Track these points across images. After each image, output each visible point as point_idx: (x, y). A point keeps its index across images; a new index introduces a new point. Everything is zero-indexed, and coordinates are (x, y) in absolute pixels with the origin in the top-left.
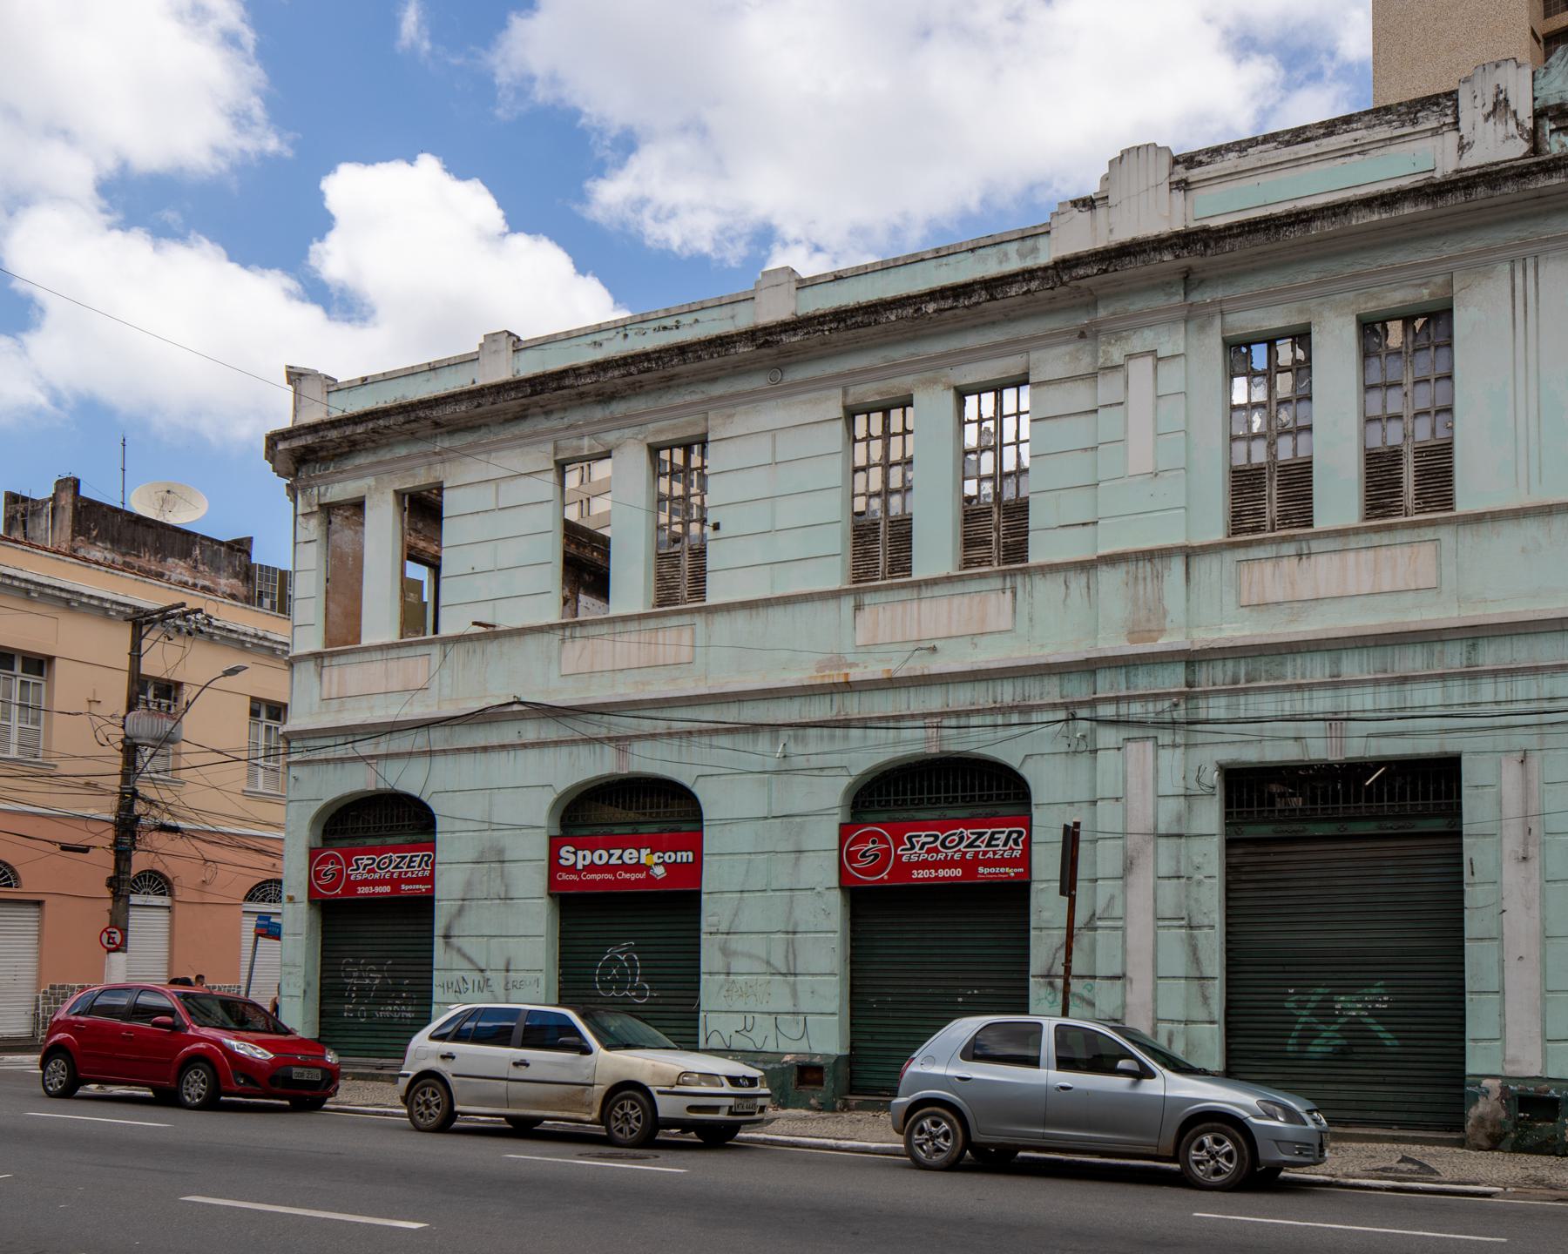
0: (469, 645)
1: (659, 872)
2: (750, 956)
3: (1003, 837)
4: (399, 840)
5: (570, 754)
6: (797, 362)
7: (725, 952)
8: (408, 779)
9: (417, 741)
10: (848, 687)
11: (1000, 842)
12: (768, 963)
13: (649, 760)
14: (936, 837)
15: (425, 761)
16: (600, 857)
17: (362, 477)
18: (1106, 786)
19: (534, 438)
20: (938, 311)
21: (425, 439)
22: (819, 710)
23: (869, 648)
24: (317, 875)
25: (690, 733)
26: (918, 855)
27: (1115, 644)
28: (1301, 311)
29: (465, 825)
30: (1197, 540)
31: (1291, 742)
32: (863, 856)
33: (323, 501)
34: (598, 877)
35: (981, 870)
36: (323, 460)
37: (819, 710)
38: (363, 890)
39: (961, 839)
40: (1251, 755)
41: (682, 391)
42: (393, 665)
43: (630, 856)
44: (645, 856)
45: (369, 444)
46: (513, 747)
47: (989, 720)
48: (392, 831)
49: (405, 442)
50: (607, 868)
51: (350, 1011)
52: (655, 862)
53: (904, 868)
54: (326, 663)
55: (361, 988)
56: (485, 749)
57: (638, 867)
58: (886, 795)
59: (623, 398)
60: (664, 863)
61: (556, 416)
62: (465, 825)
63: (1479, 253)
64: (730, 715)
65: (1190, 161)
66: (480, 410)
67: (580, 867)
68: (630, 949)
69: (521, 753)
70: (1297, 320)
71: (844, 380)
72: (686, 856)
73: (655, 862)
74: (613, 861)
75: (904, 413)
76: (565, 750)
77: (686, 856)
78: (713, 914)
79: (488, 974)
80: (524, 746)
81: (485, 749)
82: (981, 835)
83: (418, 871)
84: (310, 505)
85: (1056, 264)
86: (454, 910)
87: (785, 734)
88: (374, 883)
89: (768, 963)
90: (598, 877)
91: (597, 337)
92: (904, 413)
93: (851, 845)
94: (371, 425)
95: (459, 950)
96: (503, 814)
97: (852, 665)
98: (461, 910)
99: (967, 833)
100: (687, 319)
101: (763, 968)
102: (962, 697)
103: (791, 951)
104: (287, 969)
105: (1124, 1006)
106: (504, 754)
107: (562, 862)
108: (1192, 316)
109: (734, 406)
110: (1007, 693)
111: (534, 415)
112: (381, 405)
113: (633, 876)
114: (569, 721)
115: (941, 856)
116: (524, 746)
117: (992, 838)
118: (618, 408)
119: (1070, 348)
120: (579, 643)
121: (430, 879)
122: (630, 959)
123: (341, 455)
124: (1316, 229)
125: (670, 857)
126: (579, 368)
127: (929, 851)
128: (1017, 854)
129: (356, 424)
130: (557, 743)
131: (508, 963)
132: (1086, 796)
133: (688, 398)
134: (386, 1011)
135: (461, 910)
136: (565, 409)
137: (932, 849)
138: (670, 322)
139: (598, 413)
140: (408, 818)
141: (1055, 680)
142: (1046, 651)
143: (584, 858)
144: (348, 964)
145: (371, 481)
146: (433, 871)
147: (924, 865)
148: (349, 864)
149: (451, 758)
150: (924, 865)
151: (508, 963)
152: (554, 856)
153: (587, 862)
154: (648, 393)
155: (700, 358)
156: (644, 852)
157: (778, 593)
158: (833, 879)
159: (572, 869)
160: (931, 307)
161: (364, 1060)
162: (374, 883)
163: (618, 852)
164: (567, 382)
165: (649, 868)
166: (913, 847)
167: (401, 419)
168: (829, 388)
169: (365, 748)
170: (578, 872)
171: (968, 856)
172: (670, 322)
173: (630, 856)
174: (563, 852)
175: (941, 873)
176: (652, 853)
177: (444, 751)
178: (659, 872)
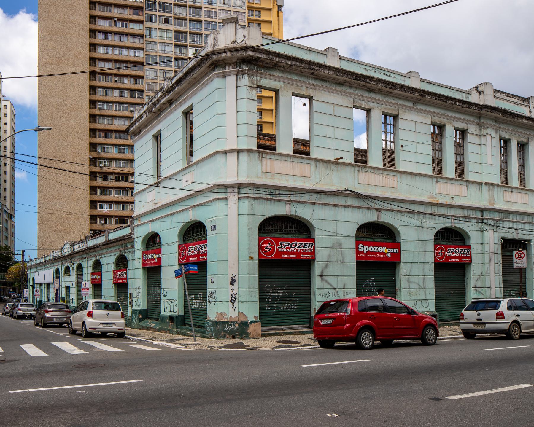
0: (325, 164)
1: (389, 255)
2: (415, 283)
3: (308, 245)
4: (290, 236)
5: (363, 212)
6: (420, 103)
7: (409, 281)
8: (304, 213)
9: (313, 198)
10: (437, 205)
11: (307, 247)
12: (419, 285)
13: (386, 218)
14: (289, 244)
15: (312, 206)
16: (371, 249)
17: (278, 81)
18: (486, 241)
19: (348, 95)
20: (459, 105)
21: (305, 76)
22: (429, 210)
23: (439, 194)
24: (262, 248)
25: (398, 211)
26: (283, 249)
27: (487, 205)
28: (510, 136)
29: (327, 233)
30: (240, 148)
31: (246, 216)
32: (266, 248)
33: (259, 84)
34: (371, 256)
35: (302, 255)
36: (259, 66)
37: (429, 210)
38: (284, 256)
39: (296, 245)
40: (509, 236)
41: (391, 98)
42: (295, 165)
43: (380, 249)
44: (385, 250)
45: (282, 69)
46: (345, 206)
47: (463, 219)
48: (287, 232)
49: (297, 74)
50: (373, 253)
51: (269, 307)
52: (388, 252)
53: (279, 254)
54: (264, 156)
55: (274, 297)
56: (334, 205)
57: (383, 253)
58: (270, 227)
59: (374, 92)
60: (390, 252)
61: (353, 89)
62: (327, 233)
63: (452, 117)
64: (410, 208)
65: (497, 91)
66: (337, 76)
67: (365, 252)
68: (373, 281)
69: (346, 209)
70: (395, 113)
71: (432, 114)
72: (396, 251)
73: (388, 252)
74: (375, 251)
75: (470, 133)
76: (361, 210)
77: (396, 251)
78: (403, 269)
79: (337, 290)
80: (348, 207)
81: (334, 205)
82: (302, 244)
83: (308, 249)
84: (253, 83)
85: (483, 105)
86: (324, 265)
87: (421, 215)
88: (289, 253)
89: (419, 285)
90: (371, 256)
91: (367, 68)
92: (470, 133)
93: (262, 244)
94: (294, 63)
95: (326, 281)
96: (341, 231)
97: (436, 198)
98: (326, 266)
99: (298, 243)
100: (392, 75)
101: (418, 287)
102: (458, 212)
103: (424, 282)
104: (251, 290)
105: (491, 294)
106: (340, 208)
107: (359, 250)
108: (497, 130)
109: (406, 109)
110: (466, 213)
111: (346, 85)
112: (286, 53)
113: (382, 256)
114: (366, 201)
115: (290, 250)
116: (348, 207)
117: (305, 245)
118: (373, 95)
119: (475, 126)
120: (364, 174)
121: (314, 253)
122: (372, 284)
123: (267, 67)
124: (519, 120)
125: (392, 250)
126: (373, 78)
127: (287, 248)
128: (312, 251)
129: (287, 59)
130: (359, 207)
131: (344, 286)
132: (480, 242)
133: (393, 101)
134: (285, 306)
135: (326, 266)
136: (356, 88)
137: (288, 248)
138: (388, 74)
139: (366, 94)
140: (301, 228)
141: (474, 212)
142: (473, 204)
143: (366, 249)
144: (268, 287)
145: (376, 105)
146: (471, 255)
147: (285, 253)
148: (277, 245)
149: (321, 207)
150: (285, 253)
151: (344, 286)
152: (357, 248)
153: (367, 250)
154: (382, 94)
155: (405, 91)
156: (384, 248)
157: (419, 172)
158: (433, 260)
159: (363, 252)
160: (458, 104)
161: (276, 327)
162: (289, 253)
163: (376, 248)
164: (368, 81)
165: (386, 254)
166: (282, 247)
167: (307, 66)
168: (428, 114)
169: (293, 198)
170: (365, 254)
171: (298, 251)
172: (388, 74)
173: (380, 249)
174: (359, 246)
175: (291, 256)
176: (387, 249)
177: (319, 203)
178: (389, 255)
